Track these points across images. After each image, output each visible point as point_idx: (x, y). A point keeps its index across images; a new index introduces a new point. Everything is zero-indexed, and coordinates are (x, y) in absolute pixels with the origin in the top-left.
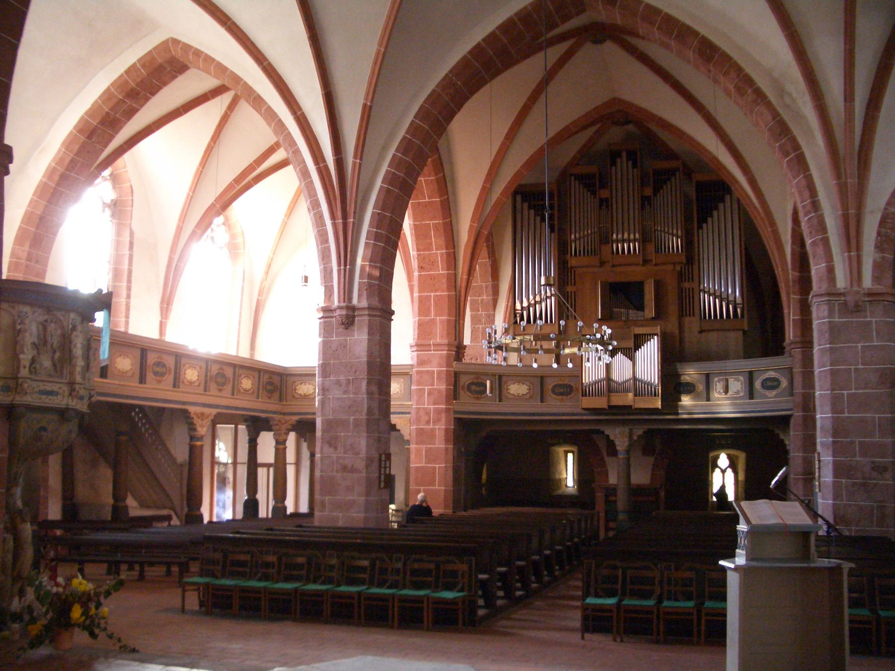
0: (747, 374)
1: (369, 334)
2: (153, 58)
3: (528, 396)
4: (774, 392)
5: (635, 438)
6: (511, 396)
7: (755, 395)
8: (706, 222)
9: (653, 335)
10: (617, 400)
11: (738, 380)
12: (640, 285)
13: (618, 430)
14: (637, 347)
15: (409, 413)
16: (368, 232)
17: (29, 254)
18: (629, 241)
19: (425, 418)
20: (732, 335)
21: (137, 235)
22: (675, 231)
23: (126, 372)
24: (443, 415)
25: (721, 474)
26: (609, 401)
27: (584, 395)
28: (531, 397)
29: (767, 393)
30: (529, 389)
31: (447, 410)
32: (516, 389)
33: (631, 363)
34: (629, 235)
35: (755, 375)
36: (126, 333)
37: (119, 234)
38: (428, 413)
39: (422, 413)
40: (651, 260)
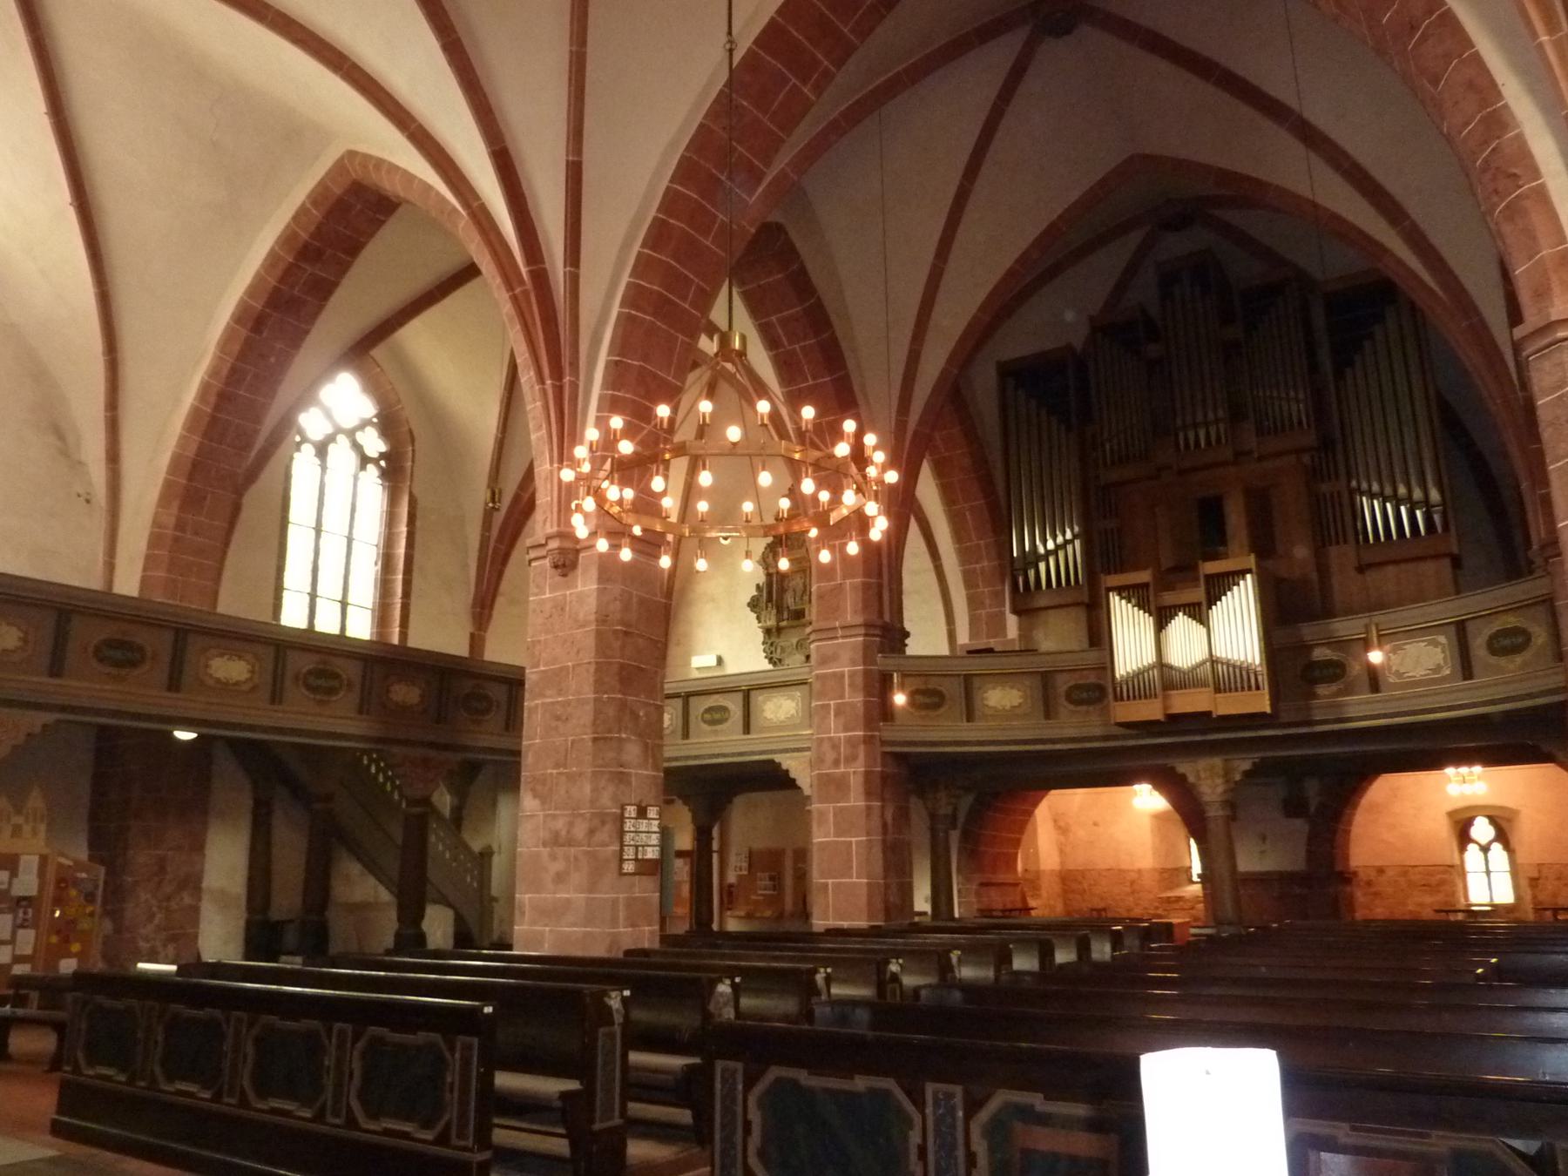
0: (1453, 629)
1: (601, 580)
2: (327, 188)
4: (1519, 659)
5: (1238, 777)
7: (1476, 670)
9: (1242, 573)
10: (1184, 703)
11: (1436, 644)
13: (1203, 764)
14: (1213, 599)
15: (808, 749)
16: (601, 398)
17: (179, 519)
18: (1207, 424)
19: (830, 756)
20: (1429, 567)
21: (422, 503)
22: (1402, 490)
23: (237, 683)
24: (861, 750)
25: (1481, 854)
26: (1165, 708)
27: (1119, 698)
29: (1502, 661)
31: (868, 741)
32: (999, 698)
33: (1204, 630)
34: (1205, 416)
35: (1470, 627)
36: (342, 635)
37: (393, 501)
38: (835, 746)
39: (826, 746)
40: (1250, 452)
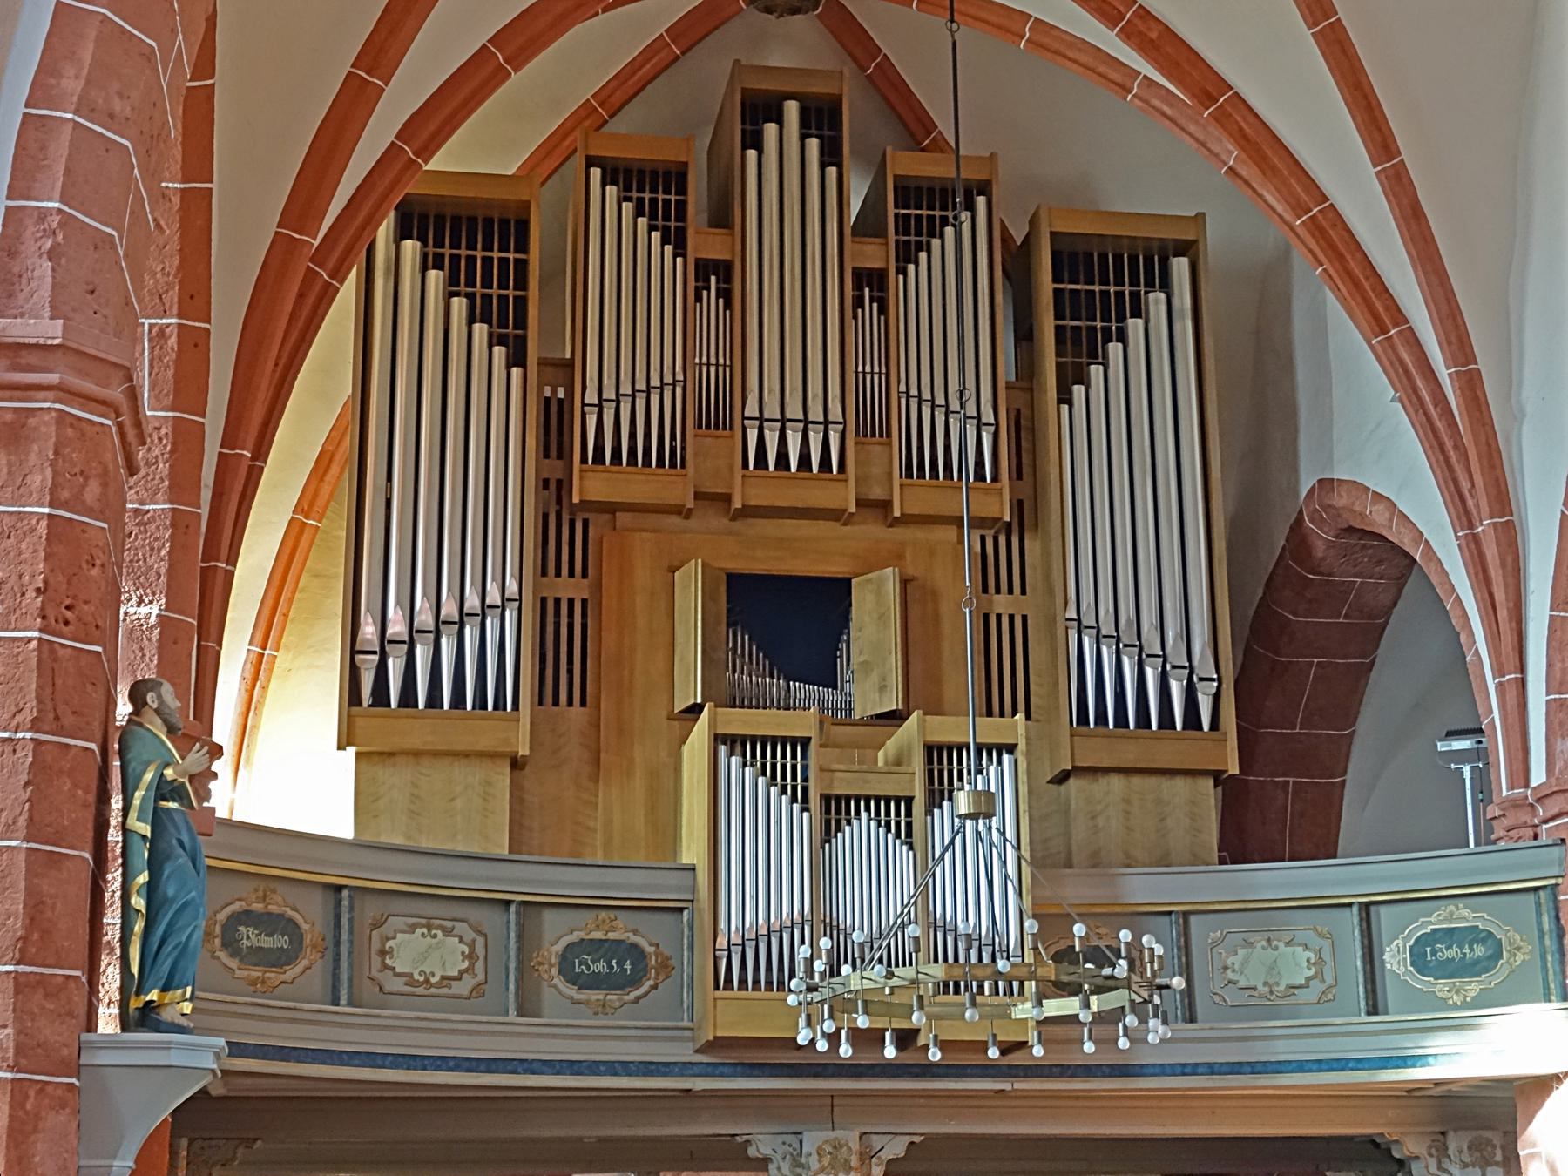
3: (462, 988)
6: (397, 985)
8: (1083, 380)
12: (838, 591)
28: (478, 991)
30: (471, 956)
32: (421, 952)
